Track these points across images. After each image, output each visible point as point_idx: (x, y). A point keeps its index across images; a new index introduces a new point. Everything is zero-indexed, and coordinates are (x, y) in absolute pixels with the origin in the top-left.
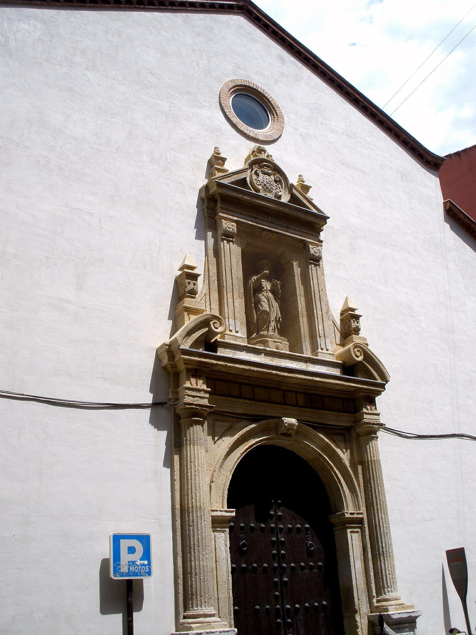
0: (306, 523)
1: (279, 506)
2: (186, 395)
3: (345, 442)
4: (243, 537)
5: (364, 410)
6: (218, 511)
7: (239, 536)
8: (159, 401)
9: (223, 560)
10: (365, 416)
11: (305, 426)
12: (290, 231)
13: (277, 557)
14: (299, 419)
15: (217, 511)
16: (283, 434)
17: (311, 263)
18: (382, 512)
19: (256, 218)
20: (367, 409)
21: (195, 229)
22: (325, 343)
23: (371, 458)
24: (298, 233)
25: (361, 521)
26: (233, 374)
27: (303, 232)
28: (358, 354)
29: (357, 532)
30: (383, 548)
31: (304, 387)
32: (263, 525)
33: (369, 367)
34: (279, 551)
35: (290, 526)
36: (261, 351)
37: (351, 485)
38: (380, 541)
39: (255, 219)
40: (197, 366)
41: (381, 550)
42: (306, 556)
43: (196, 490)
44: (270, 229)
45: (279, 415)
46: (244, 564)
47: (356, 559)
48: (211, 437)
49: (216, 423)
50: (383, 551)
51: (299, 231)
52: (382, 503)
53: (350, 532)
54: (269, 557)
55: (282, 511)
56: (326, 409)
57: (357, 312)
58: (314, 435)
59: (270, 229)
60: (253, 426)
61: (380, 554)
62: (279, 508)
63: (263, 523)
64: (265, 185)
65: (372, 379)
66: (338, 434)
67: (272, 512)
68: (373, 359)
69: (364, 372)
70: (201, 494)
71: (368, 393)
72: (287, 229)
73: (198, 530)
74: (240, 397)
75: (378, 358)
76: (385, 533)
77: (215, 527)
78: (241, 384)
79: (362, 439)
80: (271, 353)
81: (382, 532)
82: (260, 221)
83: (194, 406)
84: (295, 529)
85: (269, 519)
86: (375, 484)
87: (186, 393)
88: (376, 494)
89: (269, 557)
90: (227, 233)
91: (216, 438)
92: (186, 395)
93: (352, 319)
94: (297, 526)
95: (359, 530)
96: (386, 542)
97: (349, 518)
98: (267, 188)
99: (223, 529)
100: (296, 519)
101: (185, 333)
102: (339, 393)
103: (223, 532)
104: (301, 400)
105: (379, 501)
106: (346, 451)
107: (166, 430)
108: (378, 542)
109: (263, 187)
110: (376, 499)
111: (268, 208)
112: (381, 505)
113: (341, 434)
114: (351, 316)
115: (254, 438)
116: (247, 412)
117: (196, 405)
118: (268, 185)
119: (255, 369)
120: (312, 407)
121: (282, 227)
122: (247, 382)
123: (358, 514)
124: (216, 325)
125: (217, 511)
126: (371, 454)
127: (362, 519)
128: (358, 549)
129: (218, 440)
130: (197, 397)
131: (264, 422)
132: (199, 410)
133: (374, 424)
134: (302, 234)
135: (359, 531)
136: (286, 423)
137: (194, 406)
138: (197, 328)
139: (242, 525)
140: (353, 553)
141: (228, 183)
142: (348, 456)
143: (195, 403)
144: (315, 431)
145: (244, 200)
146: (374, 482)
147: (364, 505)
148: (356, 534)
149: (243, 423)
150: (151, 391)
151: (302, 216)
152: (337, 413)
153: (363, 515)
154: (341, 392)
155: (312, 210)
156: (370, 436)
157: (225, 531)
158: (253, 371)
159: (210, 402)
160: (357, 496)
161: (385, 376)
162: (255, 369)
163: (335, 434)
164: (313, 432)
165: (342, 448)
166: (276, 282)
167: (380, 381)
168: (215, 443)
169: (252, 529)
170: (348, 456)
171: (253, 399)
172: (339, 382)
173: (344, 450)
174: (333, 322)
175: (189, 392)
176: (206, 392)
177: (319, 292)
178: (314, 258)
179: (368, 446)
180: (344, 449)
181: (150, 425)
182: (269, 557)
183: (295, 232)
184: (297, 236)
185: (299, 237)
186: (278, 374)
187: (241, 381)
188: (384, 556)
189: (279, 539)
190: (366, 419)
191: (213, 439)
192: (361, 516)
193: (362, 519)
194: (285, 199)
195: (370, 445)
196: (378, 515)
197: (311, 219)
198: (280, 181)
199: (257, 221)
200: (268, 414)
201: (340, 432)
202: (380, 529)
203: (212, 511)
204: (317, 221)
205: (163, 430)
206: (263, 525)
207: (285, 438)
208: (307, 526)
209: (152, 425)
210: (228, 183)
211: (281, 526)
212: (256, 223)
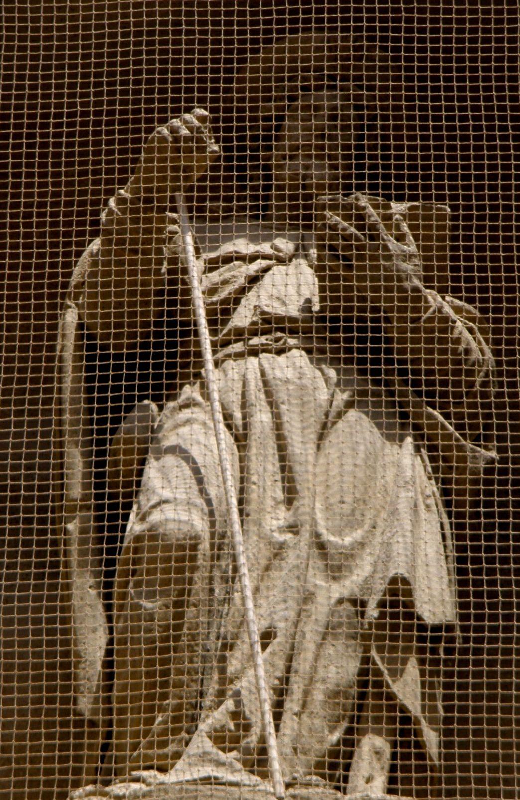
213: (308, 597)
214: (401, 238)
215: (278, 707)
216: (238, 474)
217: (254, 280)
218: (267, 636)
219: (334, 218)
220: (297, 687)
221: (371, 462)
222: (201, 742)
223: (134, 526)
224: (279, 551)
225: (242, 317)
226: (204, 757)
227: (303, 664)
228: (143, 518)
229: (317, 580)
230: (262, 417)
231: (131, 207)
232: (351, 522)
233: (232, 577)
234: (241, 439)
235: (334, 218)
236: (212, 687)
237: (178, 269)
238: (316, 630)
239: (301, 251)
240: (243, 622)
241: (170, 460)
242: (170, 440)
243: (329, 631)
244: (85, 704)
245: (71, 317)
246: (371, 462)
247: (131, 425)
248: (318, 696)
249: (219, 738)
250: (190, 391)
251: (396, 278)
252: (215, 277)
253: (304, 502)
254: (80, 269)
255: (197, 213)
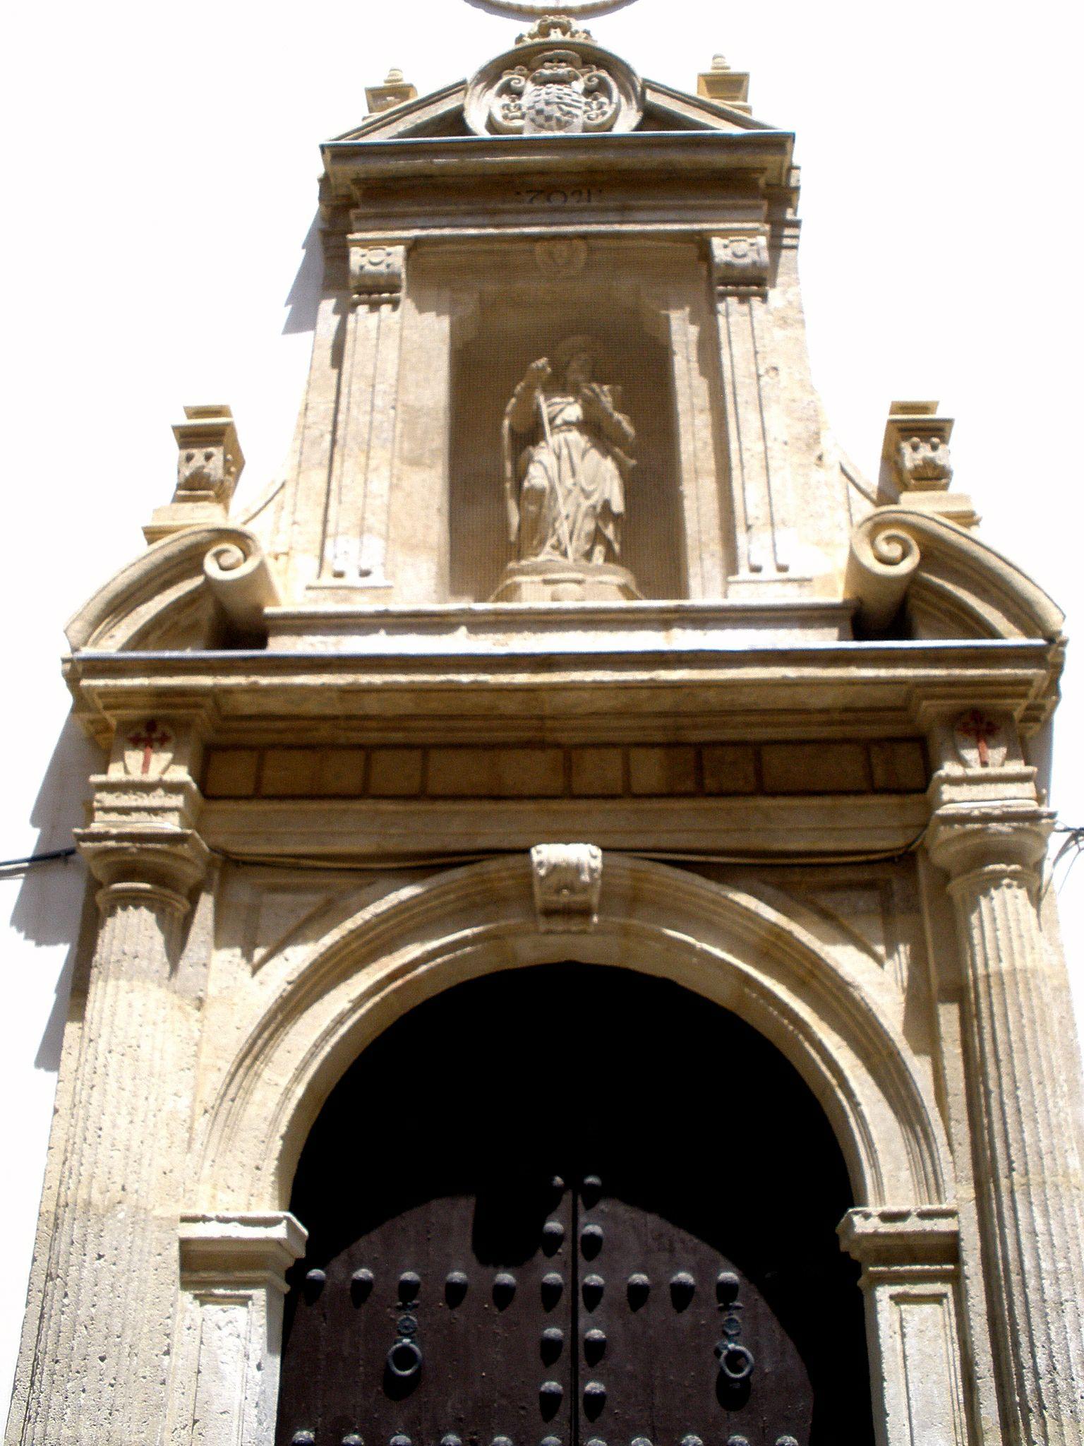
0: (723, 1261)
1: (591, 1198)
2: (99, 809)
3: (886, 913)
4: (407, 1323)
5: (950, 768)
6: (210, 1220)
7: (392, 1319)
8: (58, 846)
9: (225, 1416)
10: (948, 792)
11: (665, 869)
12: (640, 216)
13: (565, 1408)
14: (606, 844)
15: (204, 1219)
16: (550, 913)
17: (723, 296)
18: (1031, 1203)
19: (493, 213)
20: (964, 763)
21: (287, 304)
22: (774, 545)
23: (986, 965)
24: (672, 216)
25: (949, 1248)
26: (336, 718)
27: (693, 208)
28: (894, 551)
29: (937, 1299)
30: (1037, 1375)
31: (661, 722)
32: (506, 1277)
33: (949, 587)
34: (574, 1384)
35: (640, 1278)
36: (453, 620)
37: (903, 1092)
38: (1023, 1339)
39: (491, 215)
40: (152, 707)
41: (1029, 1386)
42: (713, 1405)
43: (85, 1139)
44: (554, 229)
45: (518, 842)
46: (401, 1433)
47: (924, 1427)
48: (238, 951)
49: (269, 898)
50: (1038, 1390)
51: (674, 208)
52: (1031, 1159)
53: (892, 1297)
54: (523, 1408)
55: (601, 1219)
56: (774, 794)
57: (940, 414)
58: (713, 902)
59: (554, 229)
60: (407, 892)
61: (1027, 1411)
62: (590, 1205)
63: (508, 1265)
64: (540, 112)
65: (985, 635)
66: (851, 886)
67: (553, 1225)
68: (976, 560)
69: (947, 620)
70: (100, 1156)
71: (973, 697)
72: (624, 212)
73: (66, 1295)
74: (364, 793)
75: (996, 548)
76: (1050, 1304)
77: (204, 1282)
78: (368, 749)
79: (956, 887)
80: (500, 618)
81: (1033, 1296)
82: (508, 218)
83: (111, 844)
84: (666, 1291)
85: (540, 1252)
86: (1000, 1077)
87: (98, 801)
88: (1005, 1123)
89: (524, 1404)
90: (369, 282)
91: (259, 953)
92: (99, 809)
93: (906, 439)
94: (674, 1279)
95: (947, 1288)
96: (1055, 1348)
97: (876, 1235)
98: (548, 118)
99: (242, 1292)
100: (672, 1250)
101: (98, 605)
102: (842, 723)
103: (244, 1301)
104: (649, 769)
105: (1020, 1154)
106: (890, 953)
107: (65, 942)
108: (1016, 1344)
109: (533, 120)
110: (1007, 1145)
111: (542, 172)
112: (1027, 1173)
113: (869, 886)
114: (902, 430)
115: (423, 939)
116: (391, 845)
117: (120, 837)
118: (548, 109)
119: (377, 679)
120: (700, 792)
121: (601, 213)
122: (398, 737)
123: (924, 1215)
124: (226, 560)
125: (204, 1219)
126: (984, 948)
127: (955, 1236)
128: (935, 1377)
129: (265, 960)
130: (138, 809)
131: (459, 874)
132: (131, 854)
133: (986, 818)
134: (690, 215)
135: (945, 1295)
136: (541, 864)
137: (111, 844)
138: (160, 581)
139: (409, 1276)
140: (909, 1399)
141: (390, 138)
142: (901, 969)
143: (114, 831)
144: (713, 886)
145: (444, 173)
146: (998, 1068)
147: (968, 1172)
148: (927, 1308)
149: (383, 883)
150: (36, 820)
151: (680, 158)
152: (827, 801)
153: (959, 1222)
154: (850, 716)
155: (712, 128)
156: (977, 871)
157: (249, 1297)
158: (370, 689)
159: (185, 823)
160: (928, 1136)
161: (1040, 618)
162: (377, 679)
163: (833, 888)
164: (708, 887)
165: (868, 942)
166: (593, 391)
167: (1015, 638)
168: (255, 969)
169: (455, 1293)
170: (901, 969)
171: (422, 795)
172: (791, 672)
173: (880, 949)
174: (843, 471)
175: (109, 799)
176: (173, 788)
177: (759, 377)
178: (736, 273)
179: (974, 919)
180: (877, 943)
181: (14, 929)
182: (523, 1408)
183: (658, 215)
184: (669, 227)
185: (676, 227)
186: (485, 683)
187: (374, 737)
188: (1044, 1418)
189: (580, 1332)
190: (952, 801)
191: (248, 955)
192: (943, 1225)
193: (955, 1236)
194: (627, 122)
195: (980, 913)
196: (1016, 1219)
197: (721, 159)
198: (603, 88)
199: (497, 219)
200: (483, 843)
201: (866, 875)
202: (1024, 1285)
203: (185, 1219)
204: (769, 159)
205: (54, 942)
206: (506, 1277)
207: (558, 924)
208: (729, 1275)
209: (20, 930)
210: (390, 138)
211: (595, 1279)
212: (497, 226)
213: (579, 506)
214: (606, 396)
215: (571, 538)
216: (983, 962)
217: (561, 411)
218: (567, 517)
219: (586, 391)
220: (576, 532)
221: (598, 465)
222: (547, 548)
223: (526, 484)
224: (570, 492)
225: (558, 421)
226: (548, 553)
227: (578, 525)
228: (529, 481)
229: (582, 500)
230: (565, 452)
231: (524, 389)
232: (592, 482)
233: (556, 499)
234: (559, 457)
235: (586, 391)
236: (550, 532)
237: (539, 407)
238: (159, 638)
239: (576, 402)
240: (559, 513)
241: (537, 465)
242: (536, 458)
243: (586, 515)
244: (513, 538)
245: (506, 422)
246: (598, 465)
247: (524, 455)
248: (583, 534)
249: (553, 547)
250: (542, 444)
251: (604, 409)
252: (551, 409)
253: (577, 478)
254: (509, 408)
255: (545, 391)
